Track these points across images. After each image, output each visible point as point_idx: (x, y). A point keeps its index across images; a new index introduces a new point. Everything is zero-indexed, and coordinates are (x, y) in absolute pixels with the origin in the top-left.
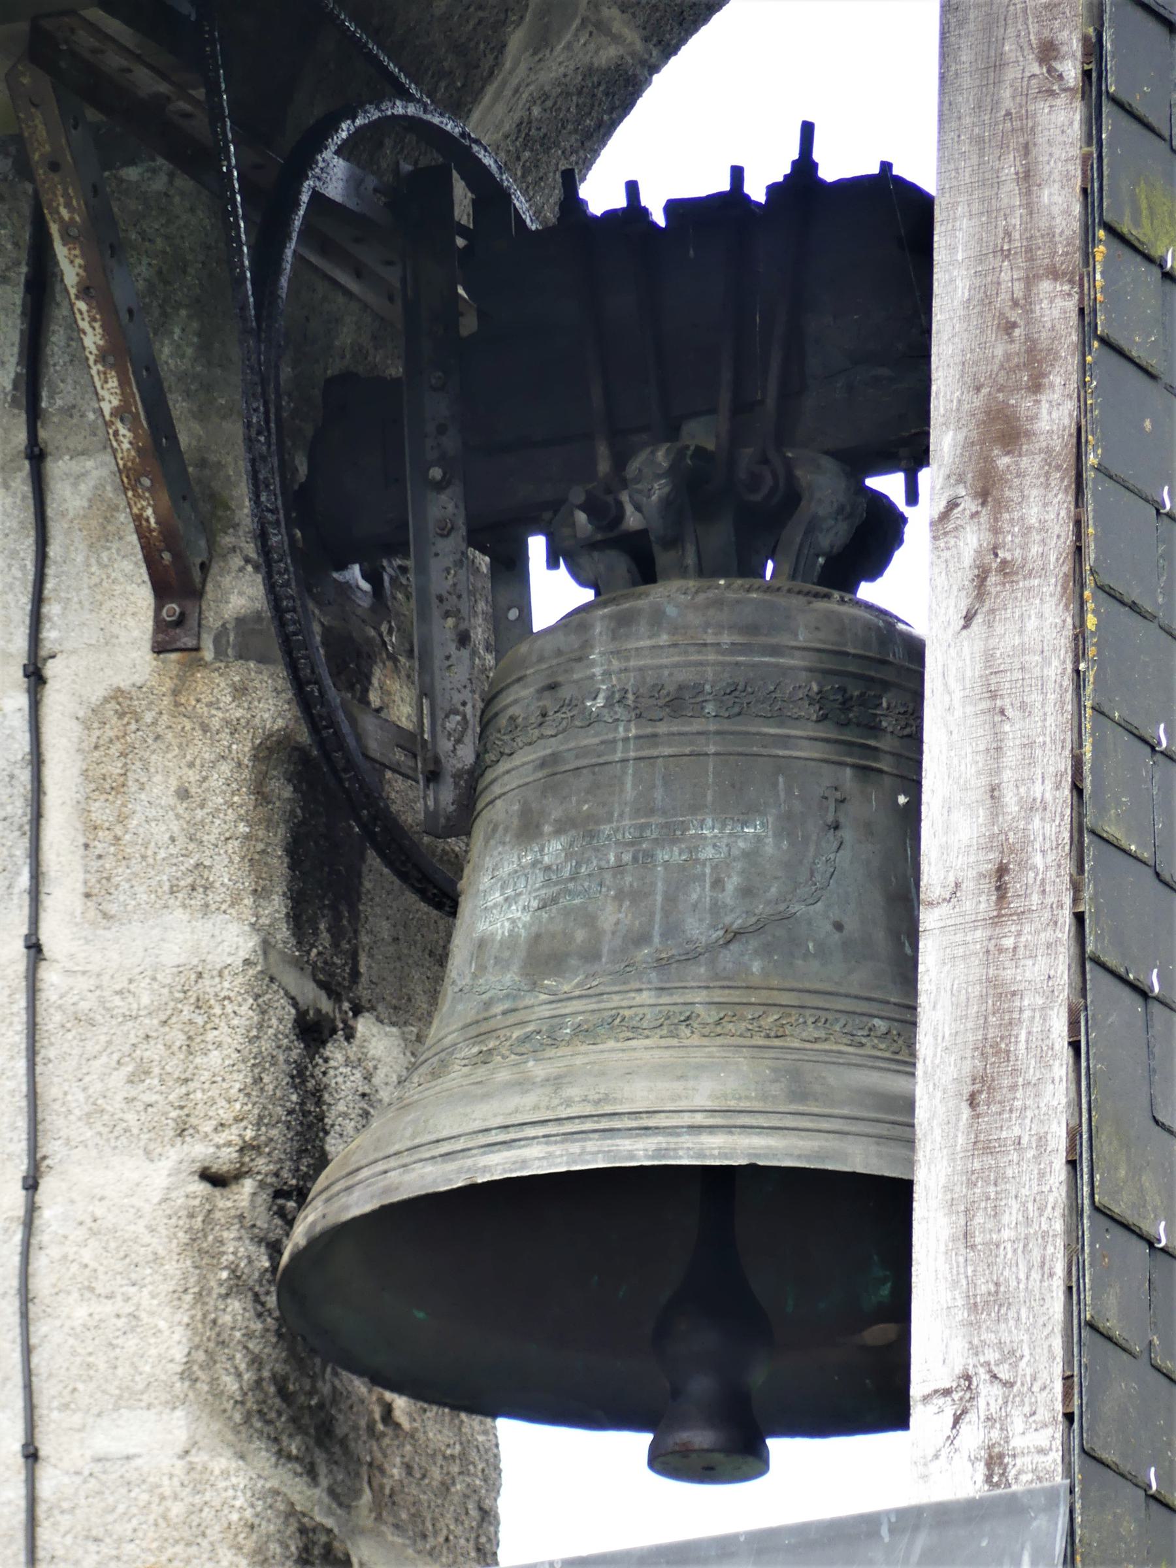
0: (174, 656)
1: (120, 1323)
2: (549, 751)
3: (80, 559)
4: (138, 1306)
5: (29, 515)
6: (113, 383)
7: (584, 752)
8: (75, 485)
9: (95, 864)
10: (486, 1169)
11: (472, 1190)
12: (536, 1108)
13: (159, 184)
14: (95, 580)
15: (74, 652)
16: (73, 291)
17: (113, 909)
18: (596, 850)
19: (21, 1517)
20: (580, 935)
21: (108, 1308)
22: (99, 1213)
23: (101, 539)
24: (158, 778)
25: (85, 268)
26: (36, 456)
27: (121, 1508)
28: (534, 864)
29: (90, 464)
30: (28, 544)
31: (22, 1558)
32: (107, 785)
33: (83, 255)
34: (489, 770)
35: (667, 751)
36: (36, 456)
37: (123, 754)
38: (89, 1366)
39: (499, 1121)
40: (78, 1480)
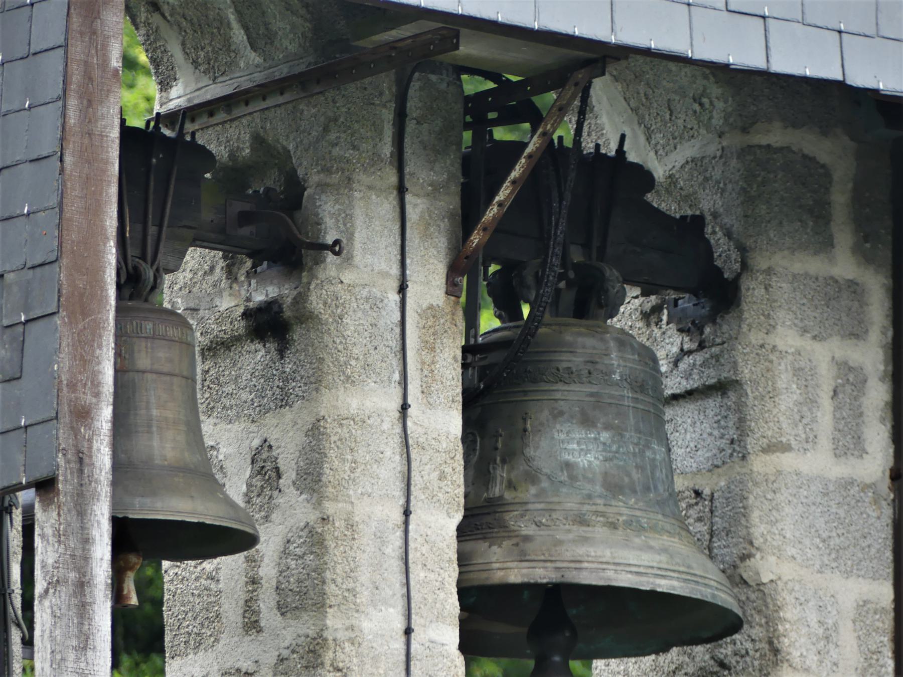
0: (453, 298)
1: (437, 584)
2: (595, 390)
3: (416, 242)
4: (444, 579)
5: (397, 214)
6: (508, 192)
7: (611, 397)
8: (414, 208)
9: (425, 379)
10: (659, 586)
11: (653, 593)
12: (660, 562)
13: (443, 86)
14: (422, 254)
15: (416, 282)
16: (525, 154)
17: (431, 401)
18: (625, 442)
19: (403, 658)
20: (626, 480)
21: (432, 576)
22: (429, 533)
23: (426, 236)
24: (447, 349)
25: (537, 148)
26: (401, 190)
27: (440, 666)
28: (595, 439)
29: (419, 201)
30: (396, 228)
31: (403, 673)
32: (429, 347)
33: (541, 144)
34: (542, 384)
35: (642, 407)
36: (401, 190)
37: (434, 334)
38: (425, 599)
39: (646, 563)
40: (423, 648)
